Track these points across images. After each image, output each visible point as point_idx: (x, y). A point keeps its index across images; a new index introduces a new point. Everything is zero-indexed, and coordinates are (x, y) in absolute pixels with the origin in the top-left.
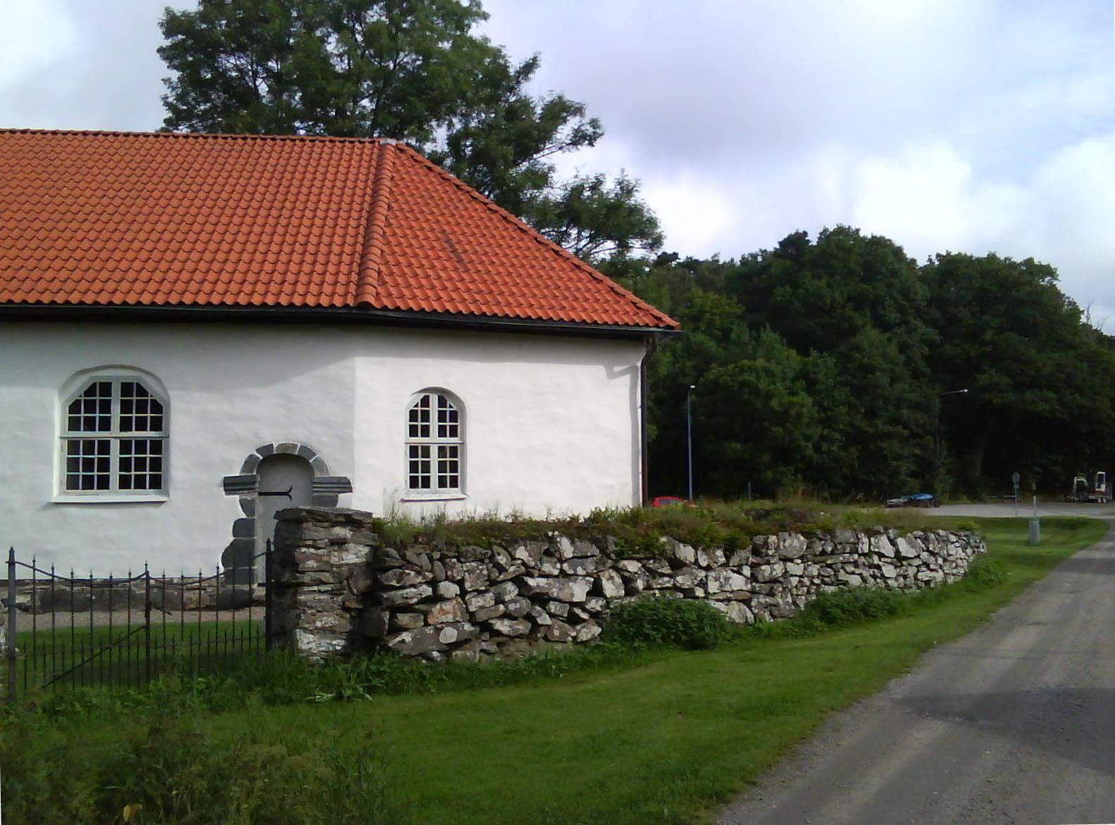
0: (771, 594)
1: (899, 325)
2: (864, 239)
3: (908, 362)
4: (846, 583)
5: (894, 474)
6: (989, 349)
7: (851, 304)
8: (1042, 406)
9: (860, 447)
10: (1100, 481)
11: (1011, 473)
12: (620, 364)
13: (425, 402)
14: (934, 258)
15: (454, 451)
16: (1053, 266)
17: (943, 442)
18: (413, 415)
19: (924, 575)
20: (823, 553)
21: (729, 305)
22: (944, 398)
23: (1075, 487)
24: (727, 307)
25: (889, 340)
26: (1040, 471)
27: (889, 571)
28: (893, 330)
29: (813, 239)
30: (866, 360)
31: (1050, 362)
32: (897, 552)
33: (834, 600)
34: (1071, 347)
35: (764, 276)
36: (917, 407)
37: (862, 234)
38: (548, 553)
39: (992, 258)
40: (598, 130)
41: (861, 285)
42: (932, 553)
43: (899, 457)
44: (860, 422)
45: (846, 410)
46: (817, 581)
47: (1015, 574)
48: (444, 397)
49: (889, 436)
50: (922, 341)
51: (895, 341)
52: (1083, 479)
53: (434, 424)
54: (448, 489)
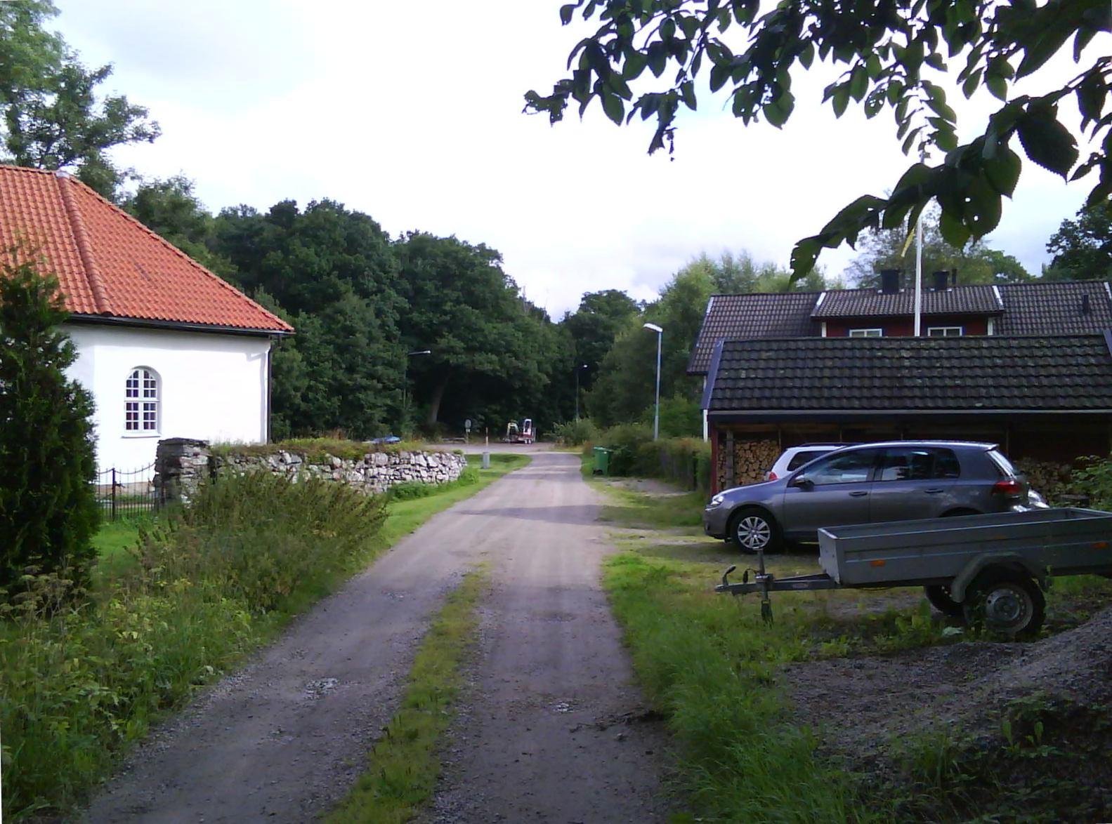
0: (373, 484)
1: (376, 293)
2: (347, 213)
3: (382, 326)
4: (405, 479)
5: (368, 420)
6: (448, 318)
7: (336, 272)
8: (487, 367)
9: (341, 397)
10: (527, 427)
11: (465, 421)
12: (254, 353)
13: (136, 375)
14: (405, 234)
15: (153, 406)
16: (500, 252)
17: (409, 394)
18: (129, 383)
19: (440, 476)
20: (395, 463)
21: (222, 264)
22: (411, 358)
23: (508, 431)
24: (221, 266)
25: (368, 305)
26: (483, 418)
27: (424, 474)
28: (371, 297)
29: (302, 208)
30: (348, 323)
31: (495, 331)
32: (428, 464)
33: (402, 487)
34: (512, 319)
35: (256, 239)
36: (389, 364)
37: (345, 208)
38: (281, 461)
39: (452, 241)
40: (158, 131)
41: (344, 254)
42: (444, 465)
43: (373, 406)
44: (341, 375)
45: (331, 365)
46: (392, 478)
47: (482, 479)
48: (148, 371)
49: (365, 388)
50: (395, 308)
51: (372, 306)
52: (515, 425)
53: (141, 389)
54: (133, 431)
